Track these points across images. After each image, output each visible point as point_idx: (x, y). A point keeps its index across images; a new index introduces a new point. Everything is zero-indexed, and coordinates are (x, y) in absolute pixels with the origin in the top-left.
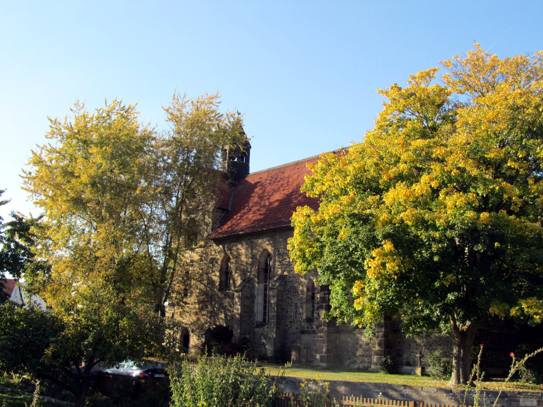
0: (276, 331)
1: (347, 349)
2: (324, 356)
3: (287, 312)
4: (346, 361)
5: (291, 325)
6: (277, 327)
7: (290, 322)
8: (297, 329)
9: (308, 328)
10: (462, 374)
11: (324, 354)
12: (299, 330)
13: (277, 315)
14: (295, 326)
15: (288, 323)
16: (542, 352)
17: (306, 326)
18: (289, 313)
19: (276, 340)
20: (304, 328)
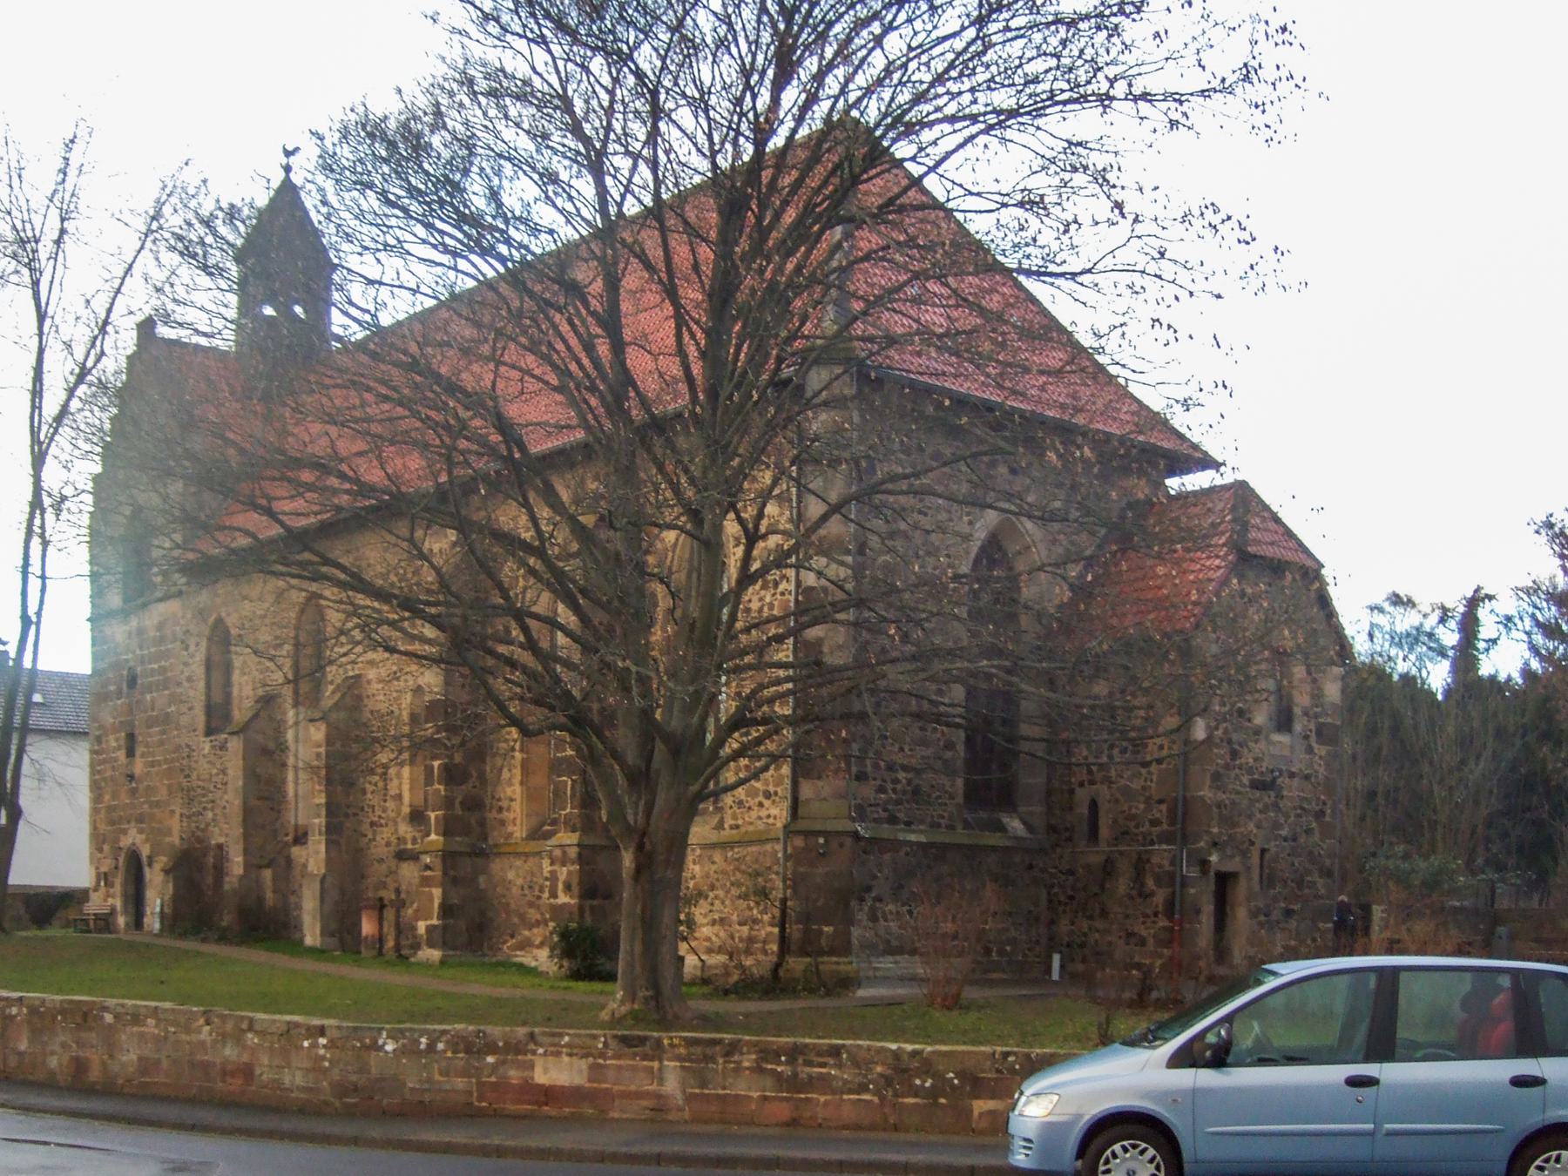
0: (327, 851)
1: (508, 904)
2: (435, 927)
3: (364, 792)
4: (505, 942)
5: (375, 833)
6: (328, 843)
7: (373, 824)
8: (388, 844)
9: (414, 840)
10: (830, 1037)
11: (435, 922)
12: (392, 848)
13: (328, 805)
14: (385, 834)
15: (365, 828)
16: (5, 987)
17: (409, 836)
18: (369, 796)
19: (329, 880)
20: (404, 841)
